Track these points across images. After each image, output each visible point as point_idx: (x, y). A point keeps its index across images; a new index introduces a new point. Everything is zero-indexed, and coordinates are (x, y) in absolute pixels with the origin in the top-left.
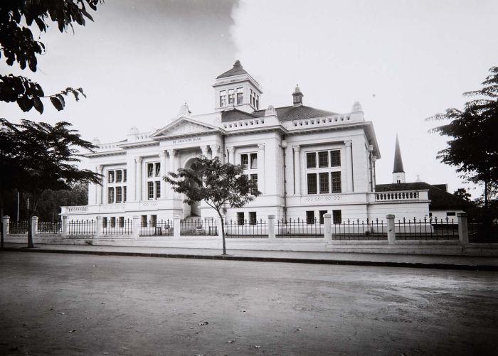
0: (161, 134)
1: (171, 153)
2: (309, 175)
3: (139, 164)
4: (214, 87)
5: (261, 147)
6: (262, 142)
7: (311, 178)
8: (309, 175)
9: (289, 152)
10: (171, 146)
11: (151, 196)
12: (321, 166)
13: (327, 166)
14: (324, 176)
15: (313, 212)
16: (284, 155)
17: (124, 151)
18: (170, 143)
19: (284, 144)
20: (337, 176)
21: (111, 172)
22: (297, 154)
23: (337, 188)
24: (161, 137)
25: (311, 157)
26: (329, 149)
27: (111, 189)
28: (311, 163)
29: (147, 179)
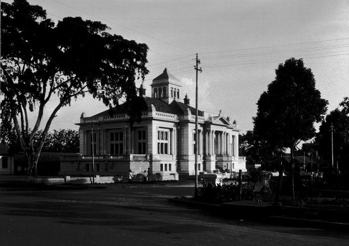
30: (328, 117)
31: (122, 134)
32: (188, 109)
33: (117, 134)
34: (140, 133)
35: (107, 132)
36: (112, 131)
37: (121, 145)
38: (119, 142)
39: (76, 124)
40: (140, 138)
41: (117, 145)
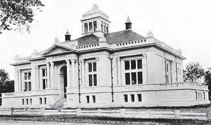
0: (46, 54)
1: (52, 64)
2: (126, 74)
3: (37, 69)
4: (82, 21)
5: (145, 56)
6: (145, 53)
7: (127, 75)
8: (126, 74)
9: (114, 61)
10: (51, 60)
11: (90, 85)
12: (138, 68)
13: (135, 69)
14: (134, 74)
15: (134, 95)
16: (112, 62)
17: (30, 62)
18: (51, 58)
19: (111, 57)
20: (140, 74)
21: (26, 74)
22: (119, 62)
23: (141, 81)
24: (46, 56)
25: (127, 63)
26: (136, 59)
27: (26, 83)
28: (127, 67)
29: (24, 81)
34: (90, 65)
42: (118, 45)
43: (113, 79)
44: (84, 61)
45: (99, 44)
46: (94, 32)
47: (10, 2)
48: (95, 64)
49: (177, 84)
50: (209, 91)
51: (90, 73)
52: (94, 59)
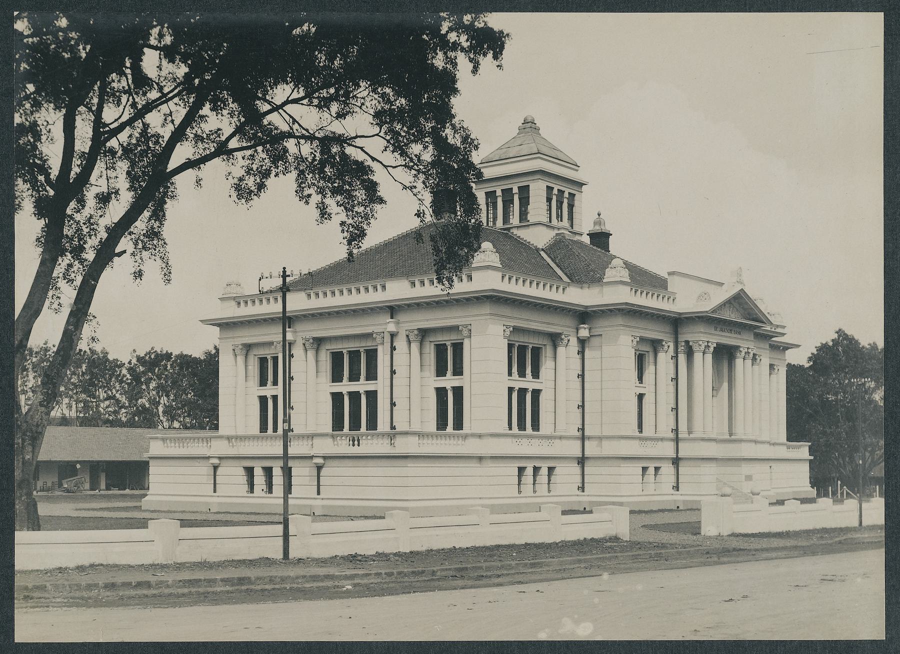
30: (84, 59)
31: (372, 355)
32: (154, 83)
33: (354, 356)
34: (441, 350)
35: (317, 351)
36: (441, 338)
37: (372, 396)
38: (362, 386)
39: (798, 346)
40: (441, 371)
41: (355, 397)
42: (413, 284)
43: (394, 408)
44: (244, 352)
45: (474, 275)
46: (518, 227)
47: (306, 149)
48: (458, 348)
49: (393, 434)
50: (812, 458)
51: (338, 388)
52: (455, 329)
